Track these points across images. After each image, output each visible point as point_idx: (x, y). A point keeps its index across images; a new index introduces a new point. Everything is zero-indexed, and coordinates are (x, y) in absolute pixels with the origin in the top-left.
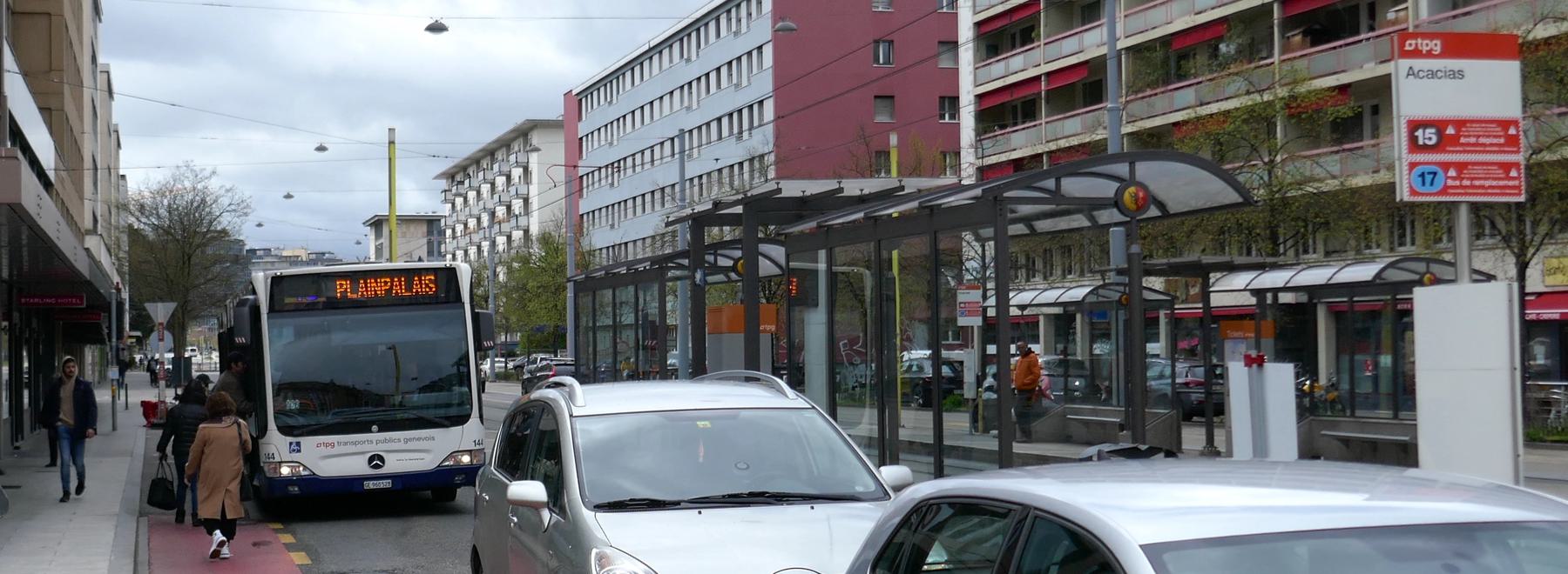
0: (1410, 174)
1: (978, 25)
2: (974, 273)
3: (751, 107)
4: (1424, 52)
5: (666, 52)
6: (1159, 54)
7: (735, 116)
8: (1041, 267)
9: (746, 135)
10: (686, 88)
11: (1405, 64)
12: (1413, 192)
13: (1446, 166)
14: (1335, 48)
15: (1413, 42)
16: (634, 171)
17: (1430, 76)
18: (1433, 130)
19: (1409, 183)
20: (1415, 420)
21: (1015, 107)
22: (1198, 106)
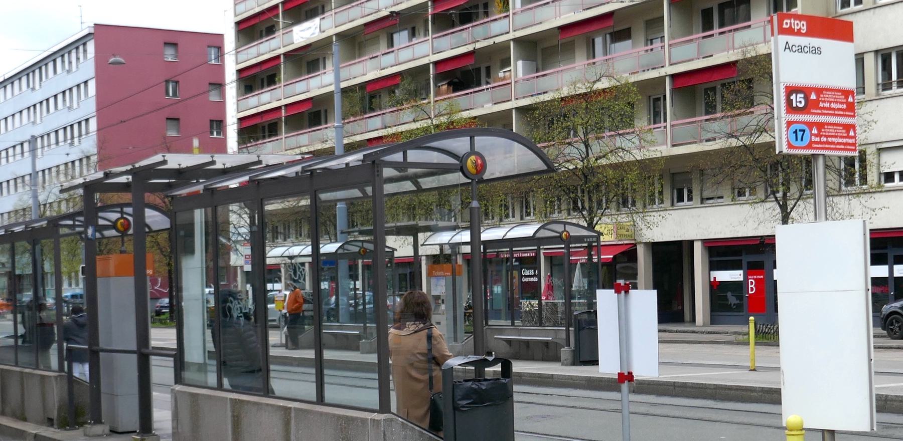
0: (787, 130)
1: (239, 71)
2: (244, 236)
3: (80, 123)
4: (796, 31)
5: (16, 83)
6: (358, 95)
7: (69, 129)
8: (282, 231)
9: (76, 140)
10: (32, 109)
11: (783, 39)
12: (790, 146)
13: (810, 125)
14: (467, 94)
15: (788, 21)
16: (7, 161)
17: (800, 50)
18: (802, 96)
19: (788, 141)
20: (659, 331)
21: (264, 127)
22: (383, 129)
